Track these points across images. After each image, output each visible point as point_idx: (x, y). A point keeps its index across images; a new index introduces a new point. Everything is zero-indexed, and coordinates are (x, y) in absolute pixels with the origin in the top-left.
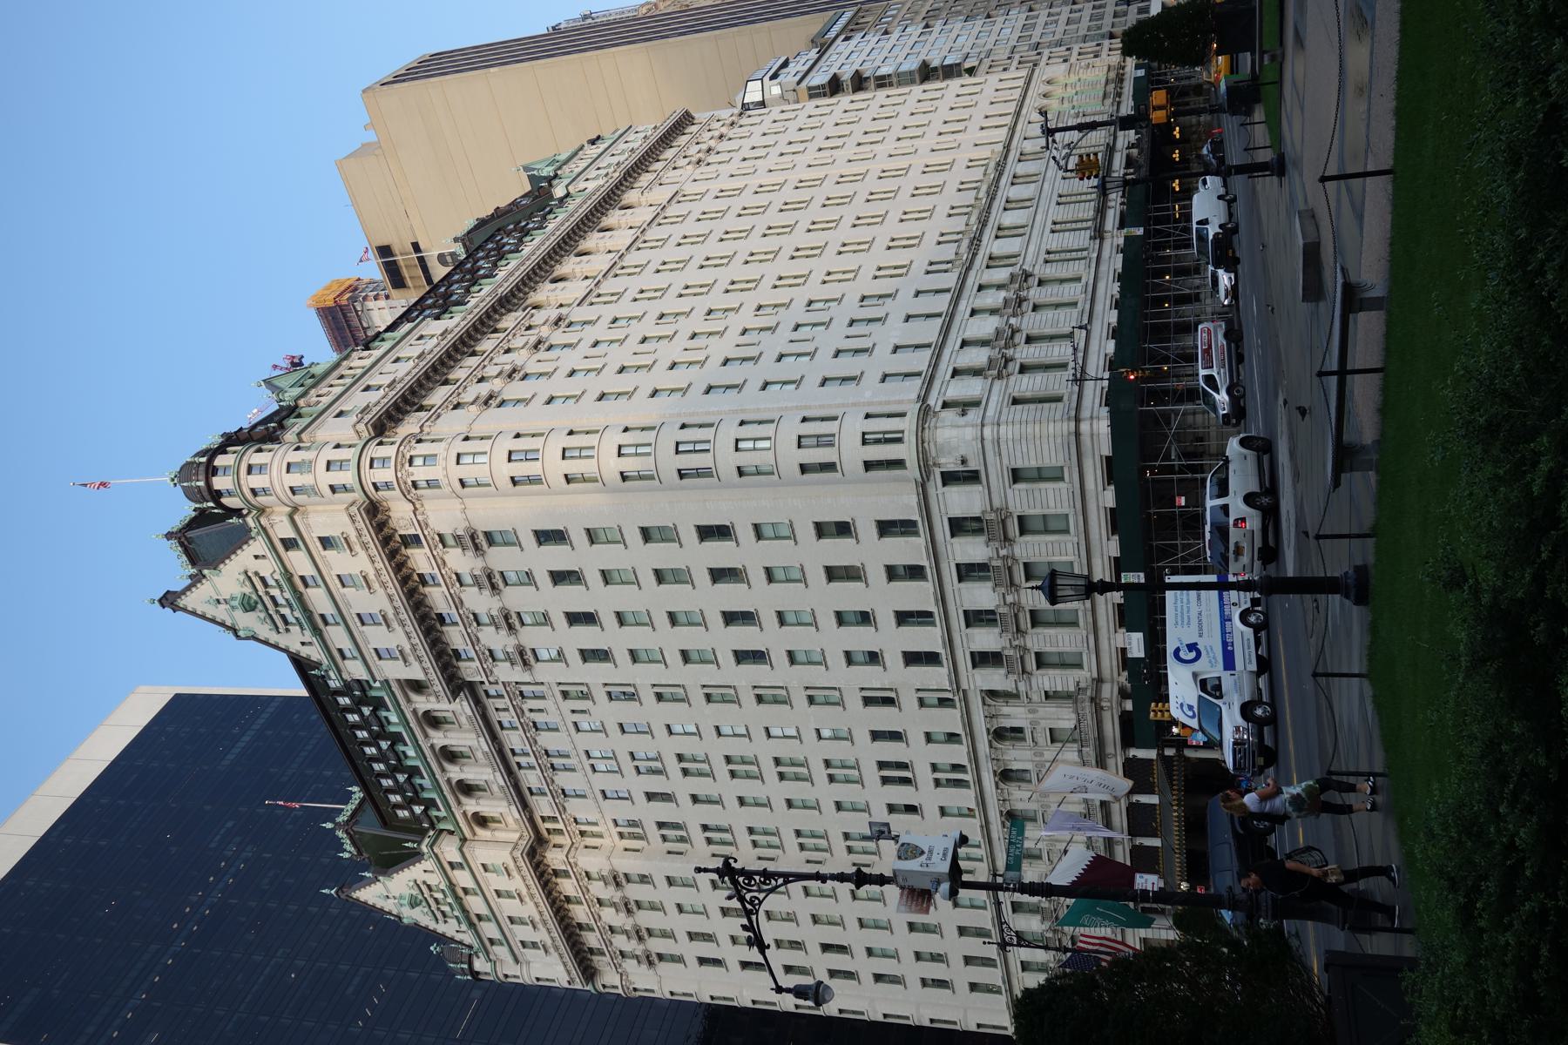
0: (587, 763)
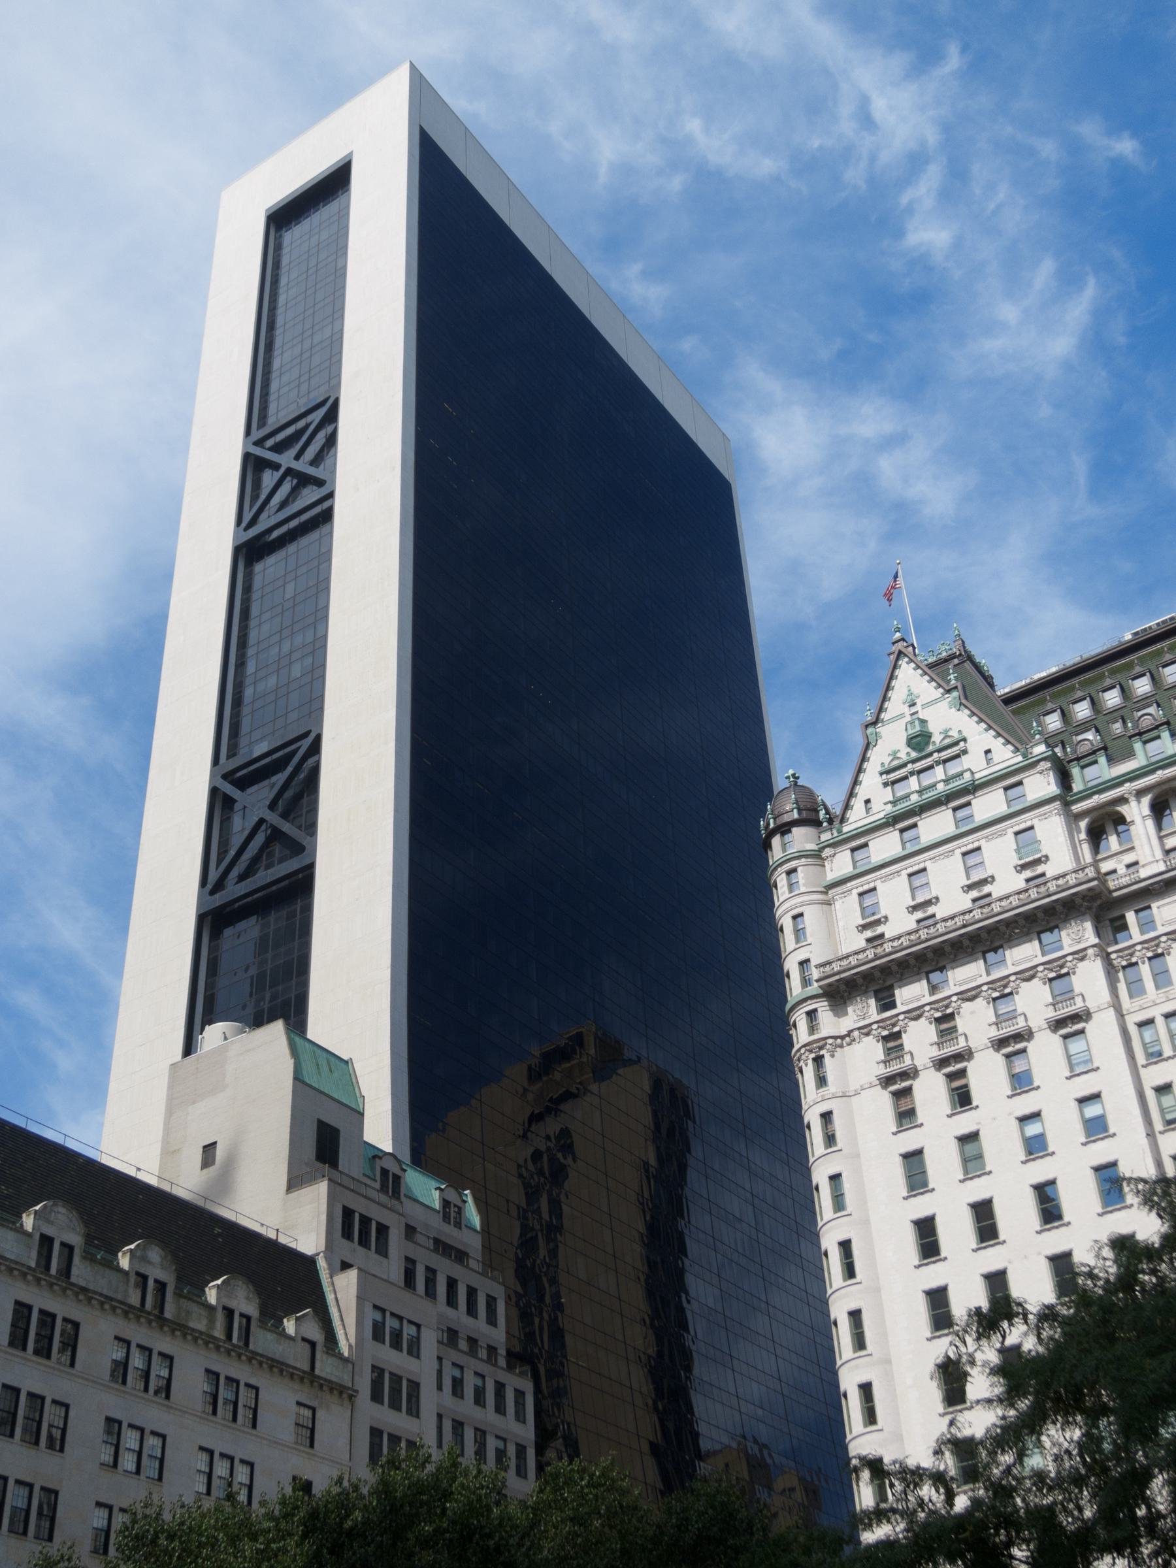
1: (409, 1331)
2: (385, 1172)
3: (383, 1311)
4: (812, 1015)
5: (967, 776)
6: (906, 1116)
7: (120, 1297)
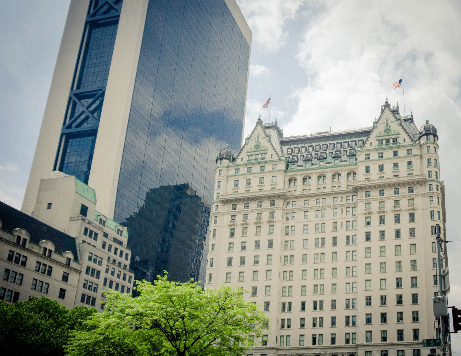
0: (320, 223)
1: (99, 259)
2: (101, 220)
7: (12, 241)
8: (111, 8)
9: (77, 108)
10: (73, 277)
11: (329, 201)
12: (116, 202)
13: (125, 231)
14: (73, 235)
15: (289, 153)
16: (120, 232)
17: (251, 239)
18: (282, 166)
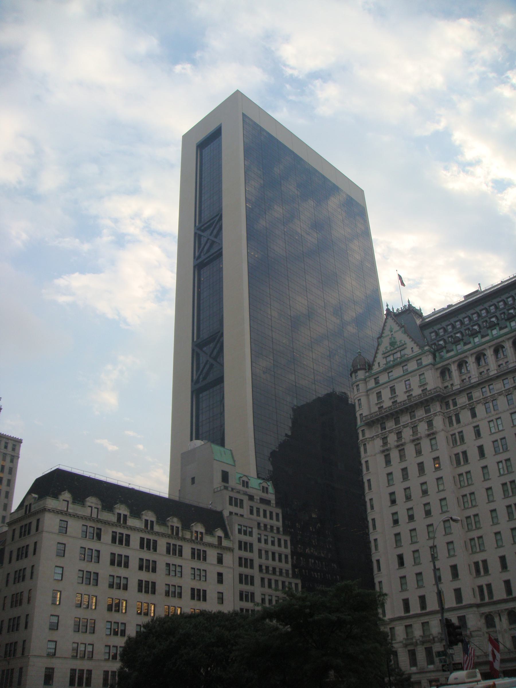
2: (243, 481)
3: (241, 525)
4: (363, 431)
5: (406, 356)
6: (388, 462)
8: (213, 242)
9: (201, 358)
10: (228, 558)
11: (498, 386)
12: (256, 452)
13: (270, 486)
14: (219, 509)
15: (433, 338)
16: (265, 490)
17: (412, 461)
18: (427, 360)
